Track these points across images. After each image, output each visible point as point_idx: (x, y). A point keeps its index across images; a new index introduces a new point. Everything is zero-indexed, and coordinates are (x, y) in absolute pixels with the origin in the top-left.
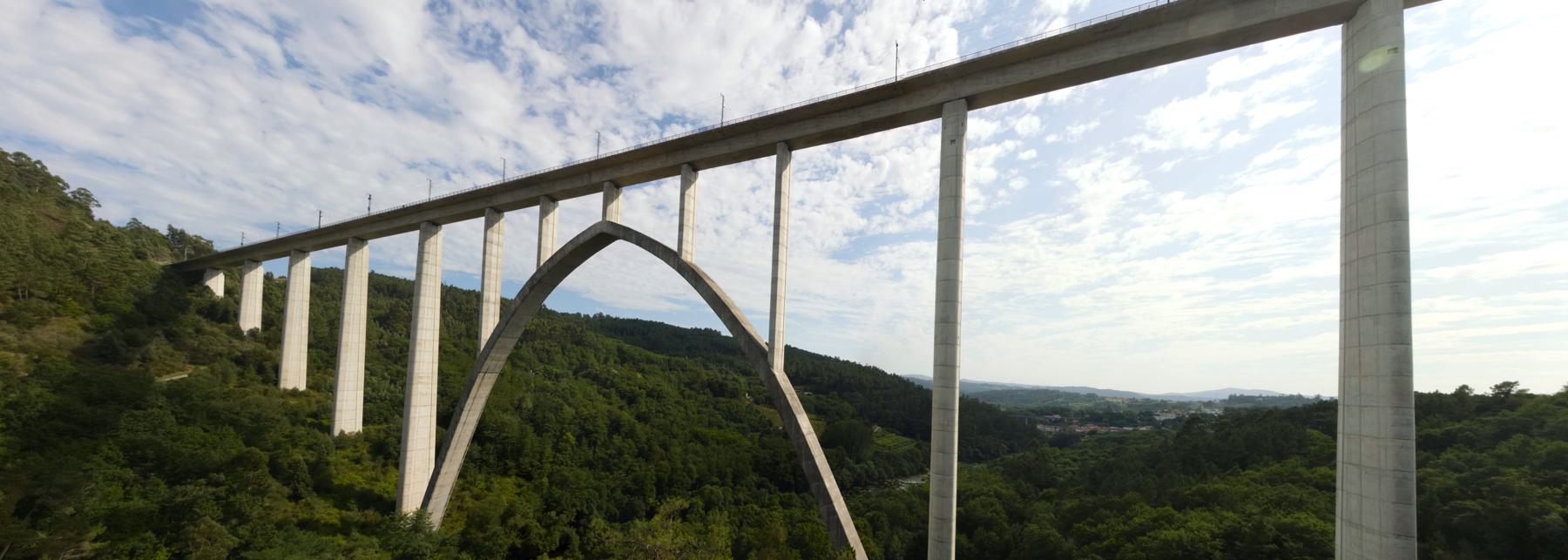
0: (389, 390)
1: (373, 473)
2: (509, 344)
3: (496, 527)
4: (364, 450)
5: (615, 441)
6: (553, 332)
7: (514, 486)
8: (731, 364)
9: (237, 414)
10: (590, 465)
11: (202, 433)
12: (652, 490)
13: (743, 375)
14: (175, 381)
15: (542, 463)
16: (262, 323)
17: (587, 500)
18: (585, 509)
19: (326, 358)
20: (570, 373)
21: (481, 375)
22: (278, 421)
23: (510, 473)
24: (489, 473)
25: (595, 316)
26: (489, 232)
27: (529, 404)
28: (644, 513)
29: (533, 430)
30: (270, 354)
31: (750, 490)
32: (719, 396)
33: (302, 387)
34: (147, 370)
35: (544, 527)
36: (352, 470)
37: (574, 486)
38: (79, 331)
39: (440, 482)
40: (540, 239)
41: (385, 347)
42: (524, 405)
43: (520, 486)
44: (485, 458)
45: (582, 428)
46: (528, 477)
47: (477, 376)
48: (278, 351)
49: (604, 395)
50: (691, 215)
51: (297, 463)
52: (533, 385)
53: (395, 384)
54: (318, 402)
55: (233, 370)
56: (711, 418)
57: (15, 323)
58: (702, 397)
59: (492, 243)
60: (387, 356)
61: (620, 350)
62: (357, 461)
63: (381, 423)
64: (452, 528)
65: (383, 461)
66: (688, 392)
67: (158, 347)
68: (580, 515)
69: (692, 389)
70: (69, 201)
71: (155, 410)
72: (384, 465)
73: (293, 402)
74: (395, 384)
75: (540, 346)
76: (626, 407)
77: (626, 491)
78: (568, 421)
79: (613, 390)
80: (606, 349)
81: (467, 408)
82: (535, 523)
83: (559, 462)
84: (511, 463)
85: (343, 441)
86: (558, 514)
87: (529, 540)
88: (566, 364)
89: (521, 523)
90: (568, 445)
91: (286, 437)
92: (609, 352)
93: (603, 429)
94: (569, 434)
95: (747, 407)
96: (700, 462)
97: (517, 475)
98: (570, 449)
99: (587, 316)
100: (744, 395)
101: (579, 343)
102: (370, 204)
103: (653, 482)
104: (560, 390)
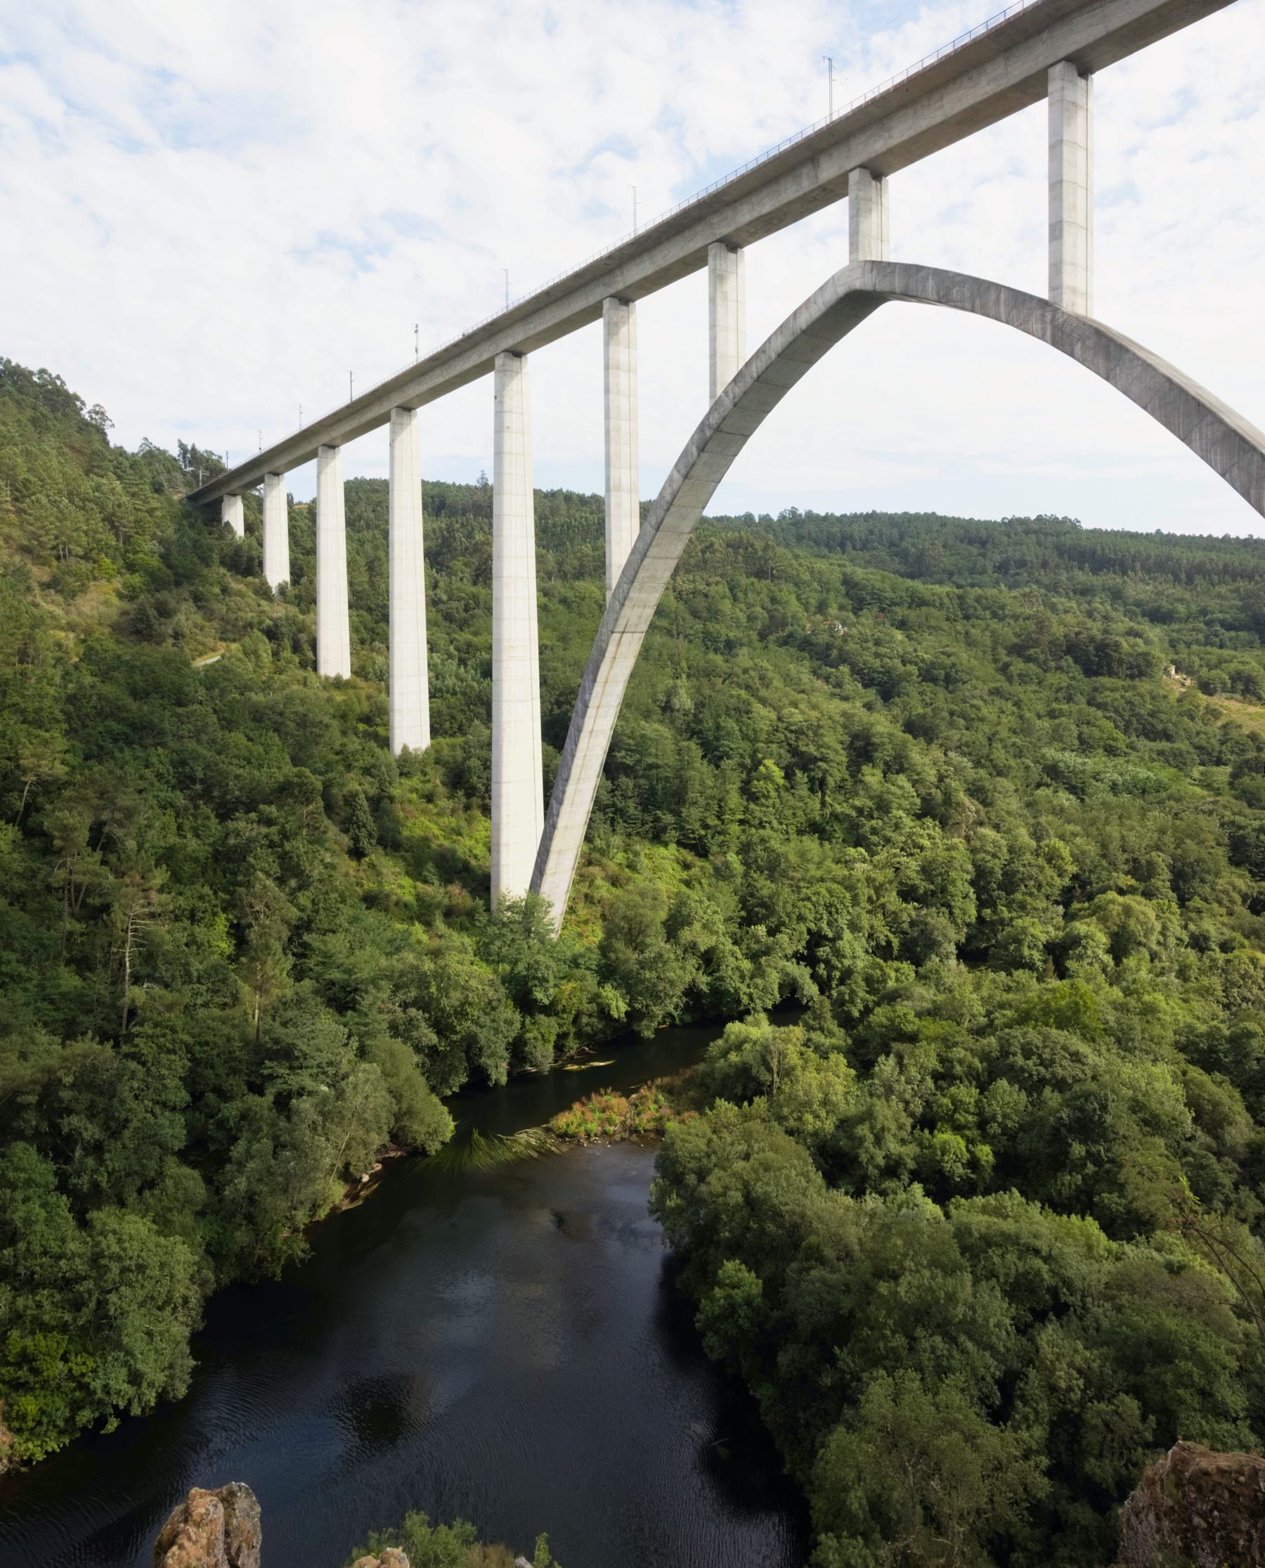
0: (458, 677)
1: (453, 820)
2: (660, 571)
3: (657, 943)
4: (436, 780)
5: (868, 779)
6: (708, 555)
7: (675, 866)
8: (1116, 595)
9: (281, 714)
10: (817, 829)
11: (244, 741)
12: (966, 897)
13: (1152, 621)
14: (212, 665)
15: (723, 822)
16: (292, 573)
17: (828, 907)
18: (824, 926)
19: (371, 625)
20: (754, 635)
21: (616, 636)
22: (327, 726)
23: (666, 837)
24: (629, 835)
25: (782, 517)
26: (612, 348)
27: (684, 701)
28: (952, 948)
29: (700, 753)
30: (303, 621)
31: (1230, 913)
32: (1097, 674)
33: (347, 675)
34: (182, 649)
35: (747, 956)
36: (424, 812)
37: (798, 875)
38: (115, 600)
39: (556, 846)
40: (713, 339)
41: (444, 603)
42: (676, 703)
43: (686, 866)
44: (620, 805)
45: (794, 751)
46: (701, 850)
47: (609, 638)
48: (312, 615)
49: (827, 679)
50: (1081, 193)
51: (354, 795)
52: (684, 664)
53: (466, 665)
54: (369, 698)
55: (265, 648)
56: (1085, 729)
57: (61, 592)
58: (1054, 678)
59: (618, 368)
60: (448, 617)
61: (847, 582)
62: (429, 798)
63: (453, 735)
64: (580, 935)
65: (464, 800)
66: (1018, 666)
67: (186, 617)
68: (816, 939)
69: (1029, 659)
70: (87, 424)
71: (196, 706)
72: (467, 808)
73: (339, 697)
74: (466, 665)
75: (689, 587)
76: (879, 703)
77: (907, 894)
78: (763, 736)
79: (845, 669)
80: (819, 582)
81: (593, 703)
82: (728, 945)
83: (757, 822)
84: (668, 818)
85: (407, 765)
86: (772, 932)
87: (721, 979)
88: (743, 618)
89: (705, 942)
90: (770, 786)
91: (337, 753)
92: (825, 587)
93: (837, 752)
94: (769, 762)
95: (1179, 700)
96: (1075, 835)
97: (679, 843)
98: (773, 794)
99: (766, 519)
100: (1166, 672)
101: (761, 574)
102: (417, 340)
103: (969, 877)
104: (739, 671)
